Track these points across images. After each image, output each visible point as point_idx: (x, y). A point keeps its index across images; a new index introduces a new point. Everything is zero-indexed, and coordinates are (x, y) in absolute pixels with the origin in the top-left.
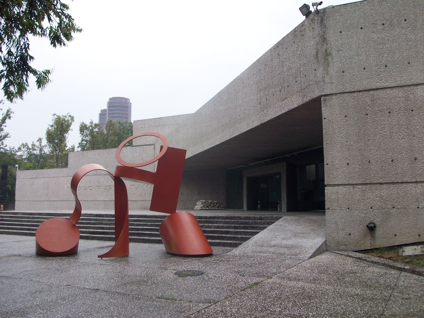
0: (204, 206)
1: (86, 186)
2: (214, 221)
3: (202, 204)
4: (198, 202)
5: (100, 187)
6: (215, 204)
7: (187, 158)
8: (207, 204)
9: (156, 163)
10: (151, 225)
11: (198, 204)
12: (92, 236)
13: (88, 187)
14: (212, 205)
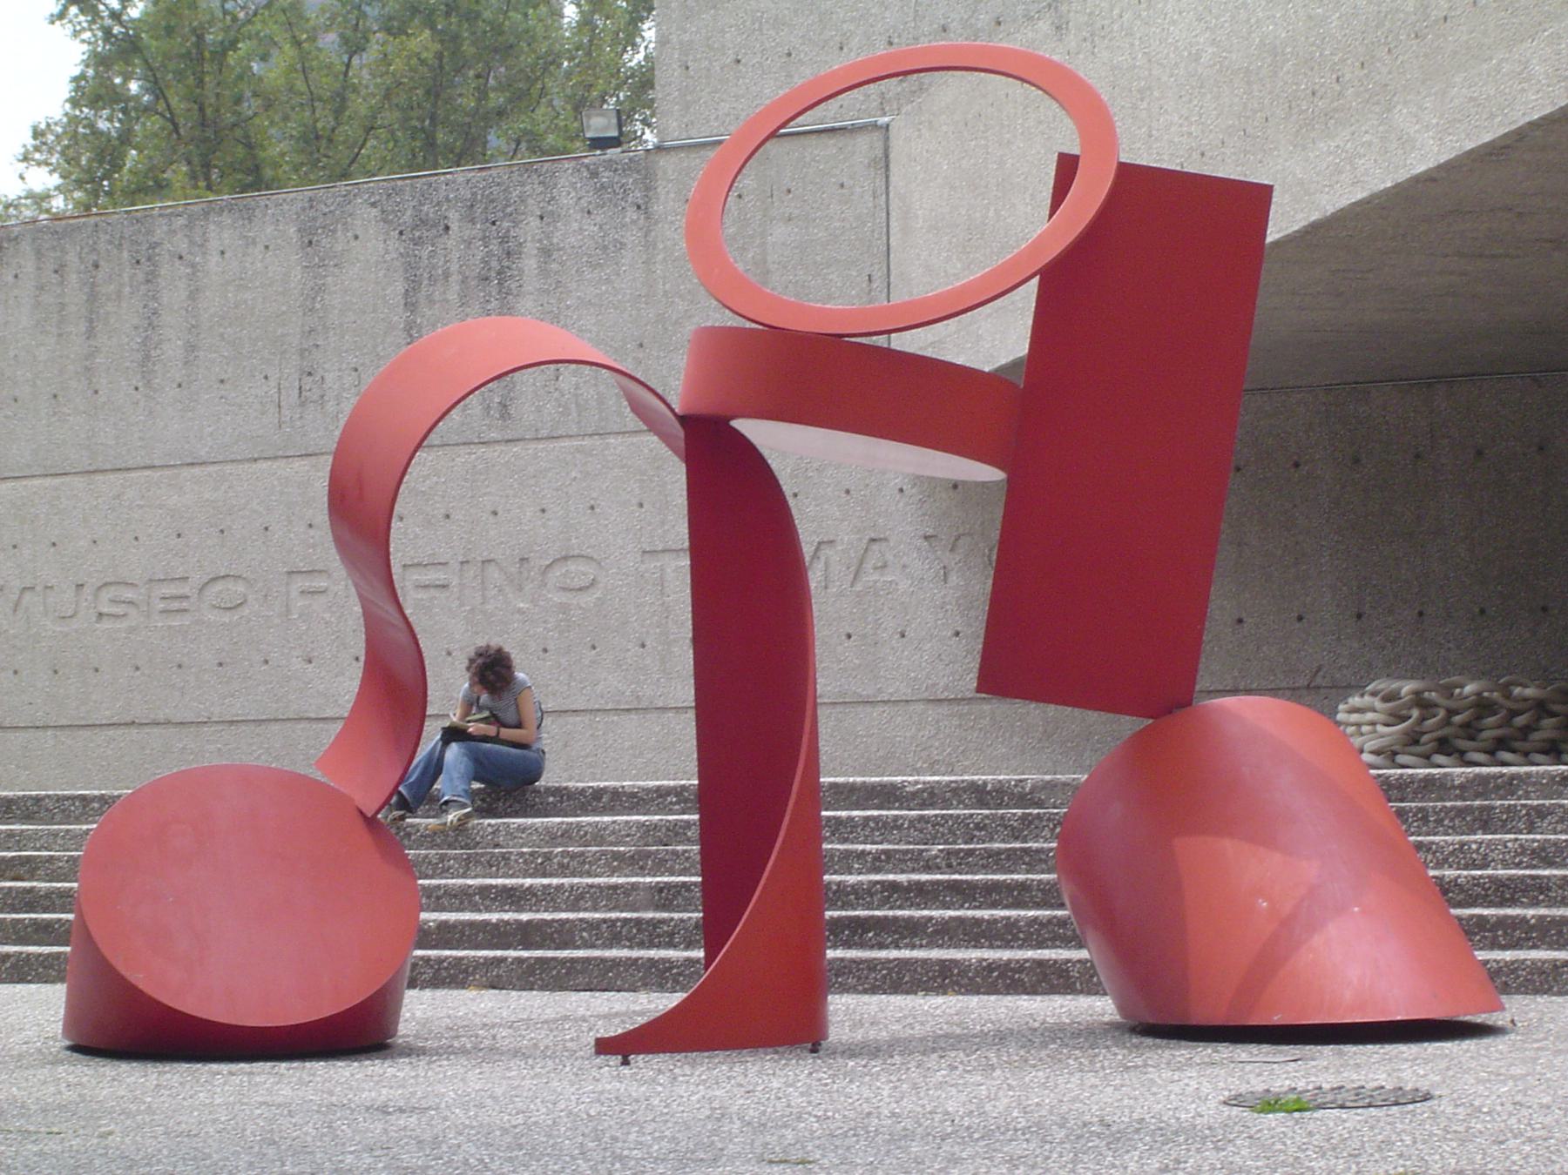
0: (1413, 739)
1: (180, 573)
2: (1509, 809)
3: (1398, 717)
4: (1355, 701)
5: (321, 583)
6: (1520, 721)
7: (1314, 230)
8: (1447, 722)
9: (1035, 281)
10: (952, 860)
11: (1355, 717)
12: (440, 961)
13: (197, 578)
14: (1491, 727)
